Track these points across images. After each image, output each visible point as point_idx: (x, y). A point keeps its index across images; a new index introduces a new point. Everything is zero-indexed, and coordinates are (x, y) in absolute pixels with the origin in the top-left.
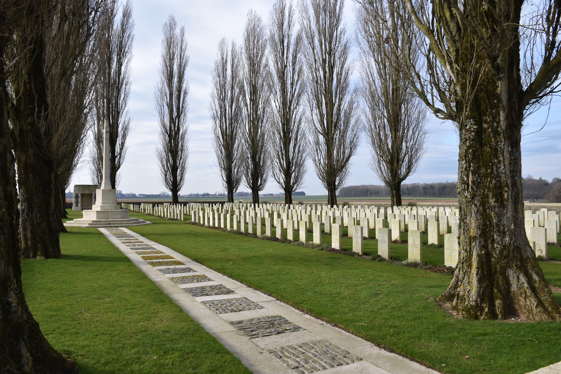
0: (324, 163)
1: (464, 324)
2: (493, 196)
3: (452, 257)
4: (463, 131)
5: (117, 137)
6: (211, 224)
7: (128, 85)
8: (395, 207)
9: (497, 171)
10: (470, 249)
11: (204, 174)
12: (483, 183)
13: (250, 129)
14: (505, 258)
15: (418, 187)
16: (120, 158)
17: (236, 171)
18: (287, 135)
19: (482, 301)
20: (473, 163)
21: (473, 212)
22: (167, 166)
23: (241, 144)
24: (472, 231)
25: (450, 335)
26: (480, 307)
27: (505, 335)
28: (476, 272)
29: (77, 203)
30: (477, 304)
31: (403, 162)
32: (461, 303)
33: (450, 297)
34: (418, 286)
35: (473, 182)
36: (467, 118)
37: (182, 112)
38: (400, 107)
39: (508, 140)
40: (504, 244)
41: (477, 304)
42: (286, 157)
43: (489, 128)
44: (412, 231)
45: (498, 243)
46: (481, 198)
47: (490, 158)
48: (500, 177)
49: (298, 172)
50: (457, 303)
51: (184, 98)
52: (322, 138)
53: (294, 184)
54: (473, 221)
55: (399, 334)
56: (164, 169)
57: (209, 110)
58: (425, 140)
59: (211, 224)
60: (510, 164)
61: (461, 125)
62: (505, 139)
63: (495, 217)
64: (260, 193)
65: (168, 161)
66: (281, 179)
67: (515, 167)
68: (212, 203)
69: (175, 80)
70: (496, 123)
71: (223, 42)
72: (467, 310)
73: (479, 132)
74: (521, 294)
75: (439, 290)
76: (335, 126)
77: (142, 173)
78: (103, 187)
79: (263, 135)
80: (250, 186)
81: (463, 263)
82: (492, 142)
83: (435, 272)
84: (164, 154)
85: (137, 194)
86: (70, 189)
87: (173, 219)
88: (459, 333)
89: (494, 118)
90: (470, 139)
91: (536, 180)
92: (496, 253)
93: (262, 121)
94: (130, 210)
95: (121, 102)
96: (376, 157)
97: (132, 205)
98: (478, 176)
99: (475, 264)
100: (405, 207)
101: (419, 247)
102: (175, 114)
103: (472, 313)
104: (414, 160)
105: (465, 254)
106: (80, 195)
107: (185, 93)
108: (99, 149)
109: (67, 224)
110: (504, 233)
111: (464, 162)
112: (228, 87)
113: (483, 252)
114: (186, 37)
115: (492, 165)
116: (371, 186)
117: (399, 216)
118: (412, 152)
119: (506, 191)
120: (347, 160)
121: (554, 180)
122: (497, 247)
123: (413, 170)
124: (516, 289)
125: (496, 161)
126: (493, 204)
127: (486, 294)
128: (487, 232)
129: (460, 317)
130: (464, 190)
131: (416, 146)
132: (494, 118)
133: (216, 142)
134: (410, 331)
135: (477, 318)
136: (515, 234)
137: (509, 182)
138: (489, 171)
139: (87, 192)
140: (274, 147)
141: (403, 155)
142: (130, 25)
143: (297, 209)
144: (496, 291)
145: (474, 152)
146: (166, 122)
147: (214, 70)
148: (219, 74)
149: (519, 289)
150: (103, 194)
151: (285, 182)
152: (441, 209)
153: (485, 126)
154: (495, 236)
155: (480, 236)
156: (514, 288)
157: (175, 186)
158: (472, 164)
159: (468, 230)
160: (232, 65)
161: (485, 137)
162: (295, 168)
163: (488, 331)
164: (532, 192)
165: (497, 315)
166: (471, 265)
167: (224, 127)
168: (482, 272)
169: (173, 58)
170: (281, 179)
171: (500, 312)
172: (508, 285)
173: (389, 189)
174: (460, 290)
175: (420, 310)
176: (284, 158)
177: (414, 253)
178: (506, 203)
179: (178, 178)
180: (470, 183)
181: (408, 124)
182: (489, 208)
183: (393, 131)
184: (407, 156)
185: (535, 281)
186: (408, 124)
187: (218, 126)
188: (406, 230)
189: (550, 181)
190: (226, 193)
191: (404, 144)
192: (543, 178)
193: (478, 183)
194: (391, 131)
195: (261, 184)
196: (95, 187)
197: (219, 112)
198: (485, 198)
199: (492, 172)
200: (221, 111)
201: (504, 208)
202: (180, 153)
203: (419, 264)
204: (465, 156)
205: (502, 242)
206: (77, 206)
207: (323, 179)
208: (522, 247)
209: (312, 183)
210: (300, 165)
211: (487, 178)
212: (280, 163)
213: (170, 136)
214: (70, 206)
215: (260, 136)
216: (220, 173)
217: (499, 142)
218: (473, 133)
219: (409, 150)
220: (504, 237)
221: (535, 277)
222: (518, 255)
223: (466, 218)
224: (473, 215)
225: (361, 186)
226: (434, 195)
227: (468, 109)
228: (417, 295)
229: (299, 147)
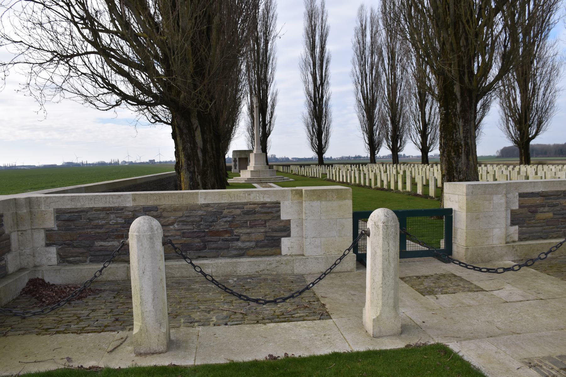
5: (267, 107)
6: (341, 180)
7: (275, 60)
11: (347, 138)
16: (270, 125)
18: (422, 98)
22: (313, 131)
23: (382, 108)
29: (235, 166)
51: (327, 67)
53: (430, 145)
59: (341, 180)
65: (313, 126)
68: (359, 164)
69: (318, 50)
71: (362, 8)
77: (289, 140)
78: (255, 151)
79: (401, 98)
80: (390, 147)
84: (309, 120)
85: (290, 158)
86: (229, 155)
87: (314, 177)
93: (401, 86)
94: (285, 172)
95: (269, 76)
96: (504, 117)
97: (281, 167)
102: (319, 82)
106: (237, 159)
107: (328, 62)
108: (252, 117)
109: (230, 181)
110: (460, 172)
112: (367, 52)
114: (327, 8)
116: (538, 145)
132: (454, 106)
139: (243, 156)
142: (273, 6)
146: (310, 90)
147: (353, 37)
148: (359, 40)
150: (255, 157)
151: (421, 143)
153: (450, 111)
160: (372, 31)
162: (431, 130)
167: (366, 92)
169: (315, 30)
179: (323, 143)
190: (369, 156)
195: (400, 146)
196: (251, 151)
197: (360, 78)
198: (449, 152)
199: (453, 138)
200: (362, 77)
202: (323, 119)
206: (235, 168)
213: (315, 103)
214: (230, 168)
215: (399, 99)
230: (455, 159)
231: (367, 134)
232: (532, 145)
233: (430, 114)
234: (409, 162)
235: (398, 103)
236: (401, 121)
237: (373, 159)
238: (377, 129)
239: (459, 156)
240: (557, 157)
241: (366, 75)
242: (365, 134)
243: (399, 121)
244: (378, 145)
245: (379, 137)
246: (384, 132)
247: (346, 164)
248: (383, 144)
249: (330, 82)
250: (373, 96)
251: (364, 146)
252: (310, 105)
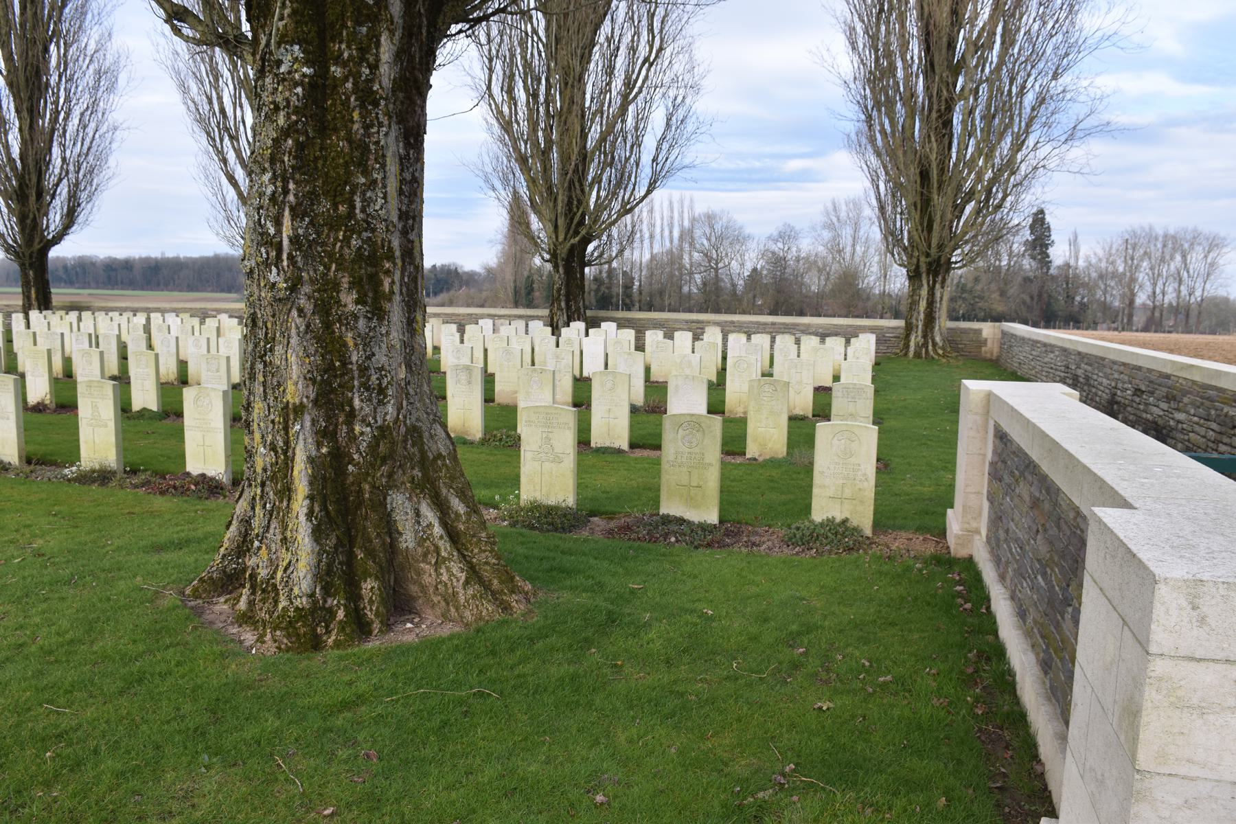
1: (286, 676)
2: (352, 285)
3: (205, 449)
4: (268, 80)
9: (363, 210)
10: (287, 443)
12: (324, 244)
14: (384, 460)
15: (93, 264)
19: (327, 591)
20: (296, 183)
21: (293, 331)
24: (290, 388)
25: (250, 732)
26: (323, 608)
27: (411, 690)
28: (305, 510)
30: (315, 602)
31: (53, 197)
32: (264, 601)
33: (229, 581)
34: (119, 549)
35: (295, 240)
36: (283, 40)
38: (46, 50)
39: (399, 123)
40: (380, 423)
41: (315, 602)
43: (346, 79)
44: (90, 384)
45: (363, 421)
46: (319, 291)
47: (349, 174)
48: (373, 230)
50: (251, 603)
54: (293, 359)
55: (77, 765)
58: (114, 146)
60: (401, 192)
61: (263, 59)
62: (390, 117)
63: (356, 345)
67: (411, 202)
70: (369, 66)
72: (288, 624)
73: (319, 88)
74: (425, 555)
75: (187, 558)
81: (263, 485)
82: (353, 122)
83: (163, 493)
88: (278, 715)
89: (363, 51)
90: (288, 106)
92: (358, 450)
98: (311, 223)
99: (301, 487)
100: (63, 313)
101: (112, 425)
103: (302, 630)
104: (84, 196)
105: (271, 458)
110: (382, 391)
111: (267, 177)
113: (324, 450)
115: (353, 193)
118: (78, 172)
119: (388, 272)
122: (362, 434)
123: (81, 219)
124: (411, 545)
125: (363, 180)
126: (351, 307)
127: (338, 574)
128: (333, 391)
129: (270, 647)
130: (267, 264)
131: (91, 158)
132: (363, 51)
134: (116, 746)
135: (316, 644)
136: (407, 394)
137: (396, 244)
138: (342, 209)
141: (53, 180)
144: (361, 556)
145: (300, 147)
149: (421, 542)
152: (156, 318)
153: (336, 71)
154: (357, 402)
155: (315, 402)
156: (408, 540)
158: (291, 186)
159: (279, 385)
161: (334, 105)
163: (362, 687)
165: (370, 624)
166: (289, 490)
168: (324, 508)
171: (377, 615)
172: (390, 537)
173: (16, 267)
174: (258, 562)
175: (141, 647)
177: (98, 441)
178: (387, 306)
180: (286, 242)
181: (68, 99)
182: (339, 321)
183: (25, 114)
184: (65, 181)
185: (457, 515)
186: (68, 99)
188: (69, 374)
191: (56, 151)
193: (311, 244)
194: (17, 111)
198: (328, 288)
199: (351, 214)
201: (381, 319)
203: (114, 473)
204: (273, 160)
205: (375, 418)
208: (424, 428)
211: (337, 231)
217: (372, 126)
218: (299, 90)
219: (71, 168)
220: (381, 403)
221: (458, 506)
222: (415, 450)
223: (271, 350)
224: (294, 341)
226: (131, 284)
227: (287, 11)
228: (122, 585)
230: (362, 323)
232: (61, 260)
239: (378, 313)
240: (10, 286)
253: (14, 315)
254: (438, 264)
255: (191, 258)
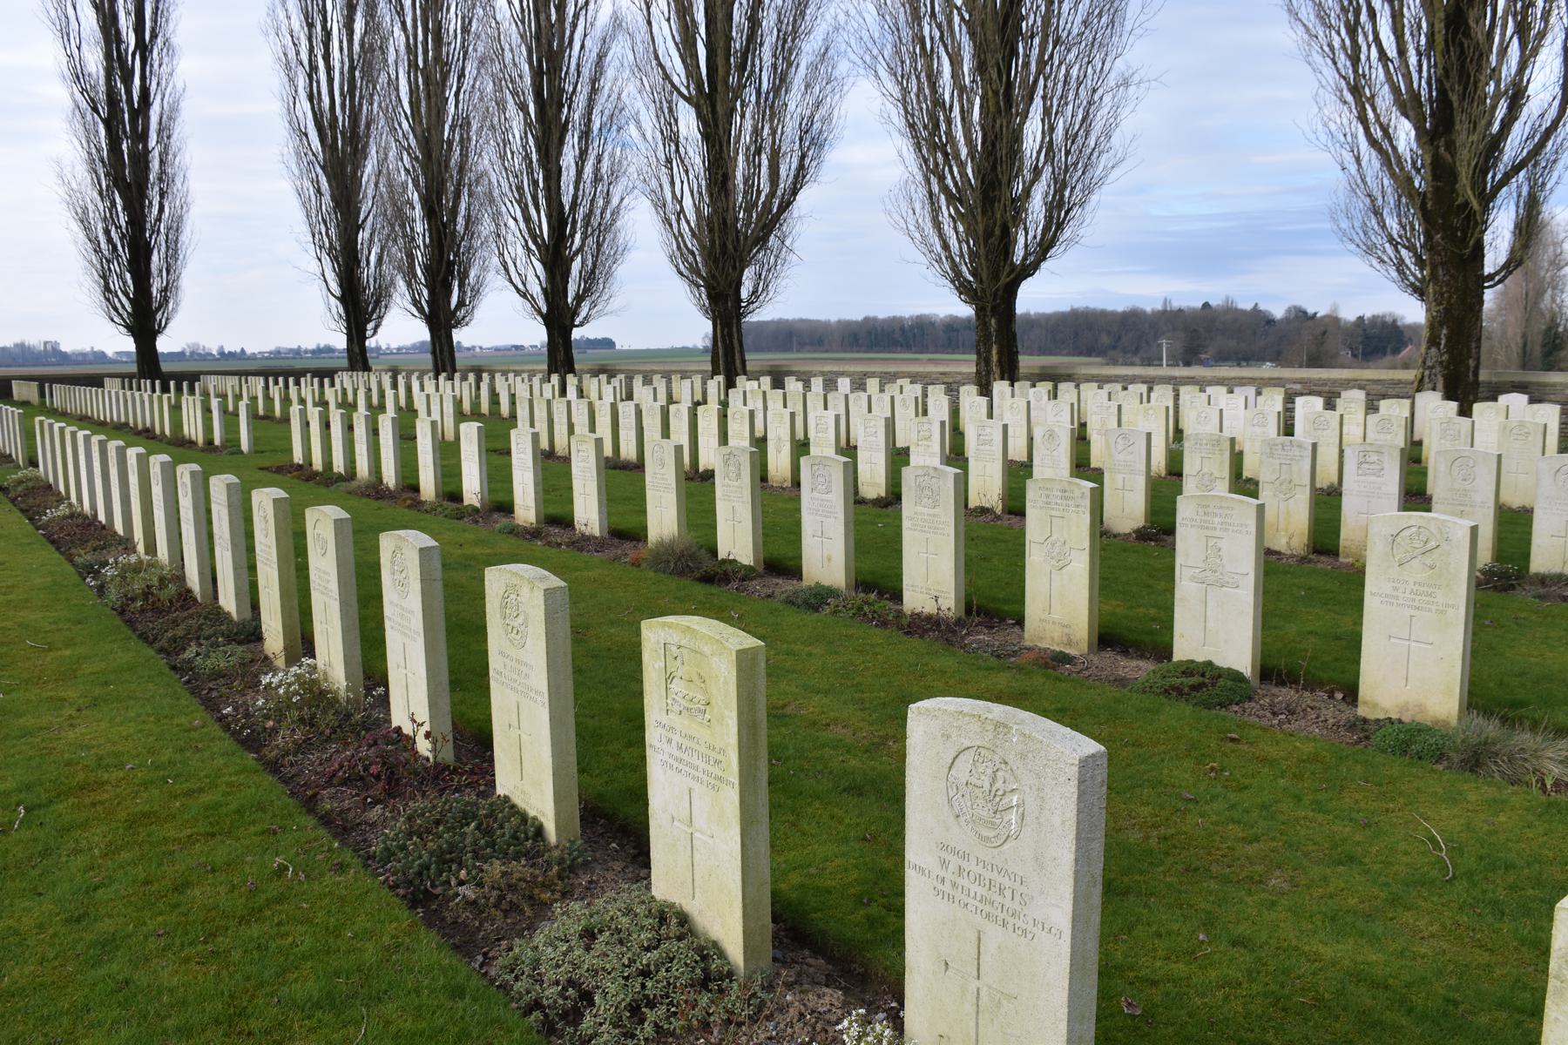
0: (698, 211)
8: (1000, 387)
11: (254, 280)
13: (413, 91)
15: (932, 324)
17: (373, 259)
18: (550, 112)
22: (110, 240)
23: (388, 161)
37: (154, 36)
42: (548, 198)
49: (596, 257)
52: (688, 122)
53: (580, 299)
56: (98, 250)
57: (267, 34)
64: (460, 336)
65: (109, 220)
66: (531, 279)
76: (742, 67)
79: (465, 124)
85: (110, 353)
91: (1243, 312)
93: (461, 76)
97: (258, 384)
116: (802, 321)
117: (1021, 418)
120: (786, 205)
121: (1289, 310)
133: (298, 154)
140: (503, 157)
143: (594, 396)
151: (545, 291)
157: (144, 320)
162: (583, 240)
164: (1232, 343)
170: (531, 279)
176: (542, 202)
187: (303, 95)
189: (1278, 312)
192: (1262, 307)
195: (461, 304)
197: (304, 44)
200: (310, 39)
202: (154, 194)
207: (691, 274)
209: (648, 300)
210: (601, 230)
212: (527, 219)
215: (452, 128)
216: (314, 266)
225: (772, 322)
229: (599, 159)
231: (334, 259)
233: (580, 172)
234: (510, 360)
235: (450, 143)
236: (463, 206)
237: (358, 357)
238: (371, 240)
241: (328, 34)
242: (326, 260)
243: (454, 212)
244: (378, 302)
245: (379, 276)
246: (397, 251)
247: (247, 373)
248: (396, 297)
249: (175, 40)
250: (354, 116)
251: (322, 307)
252: (89, 133)
253: (962, 389)
254: (1368, 314)
255: (1044, 315)
